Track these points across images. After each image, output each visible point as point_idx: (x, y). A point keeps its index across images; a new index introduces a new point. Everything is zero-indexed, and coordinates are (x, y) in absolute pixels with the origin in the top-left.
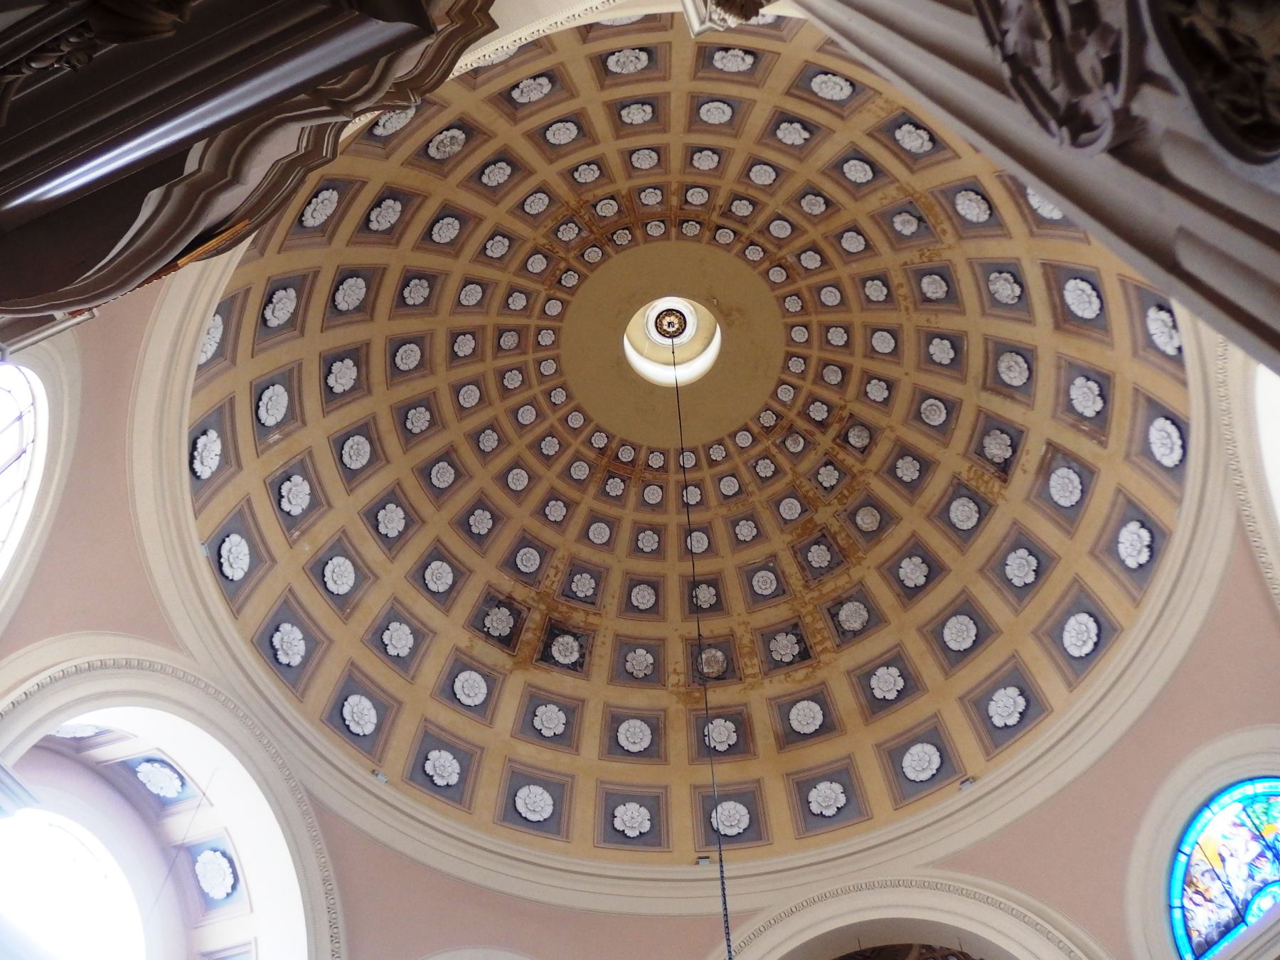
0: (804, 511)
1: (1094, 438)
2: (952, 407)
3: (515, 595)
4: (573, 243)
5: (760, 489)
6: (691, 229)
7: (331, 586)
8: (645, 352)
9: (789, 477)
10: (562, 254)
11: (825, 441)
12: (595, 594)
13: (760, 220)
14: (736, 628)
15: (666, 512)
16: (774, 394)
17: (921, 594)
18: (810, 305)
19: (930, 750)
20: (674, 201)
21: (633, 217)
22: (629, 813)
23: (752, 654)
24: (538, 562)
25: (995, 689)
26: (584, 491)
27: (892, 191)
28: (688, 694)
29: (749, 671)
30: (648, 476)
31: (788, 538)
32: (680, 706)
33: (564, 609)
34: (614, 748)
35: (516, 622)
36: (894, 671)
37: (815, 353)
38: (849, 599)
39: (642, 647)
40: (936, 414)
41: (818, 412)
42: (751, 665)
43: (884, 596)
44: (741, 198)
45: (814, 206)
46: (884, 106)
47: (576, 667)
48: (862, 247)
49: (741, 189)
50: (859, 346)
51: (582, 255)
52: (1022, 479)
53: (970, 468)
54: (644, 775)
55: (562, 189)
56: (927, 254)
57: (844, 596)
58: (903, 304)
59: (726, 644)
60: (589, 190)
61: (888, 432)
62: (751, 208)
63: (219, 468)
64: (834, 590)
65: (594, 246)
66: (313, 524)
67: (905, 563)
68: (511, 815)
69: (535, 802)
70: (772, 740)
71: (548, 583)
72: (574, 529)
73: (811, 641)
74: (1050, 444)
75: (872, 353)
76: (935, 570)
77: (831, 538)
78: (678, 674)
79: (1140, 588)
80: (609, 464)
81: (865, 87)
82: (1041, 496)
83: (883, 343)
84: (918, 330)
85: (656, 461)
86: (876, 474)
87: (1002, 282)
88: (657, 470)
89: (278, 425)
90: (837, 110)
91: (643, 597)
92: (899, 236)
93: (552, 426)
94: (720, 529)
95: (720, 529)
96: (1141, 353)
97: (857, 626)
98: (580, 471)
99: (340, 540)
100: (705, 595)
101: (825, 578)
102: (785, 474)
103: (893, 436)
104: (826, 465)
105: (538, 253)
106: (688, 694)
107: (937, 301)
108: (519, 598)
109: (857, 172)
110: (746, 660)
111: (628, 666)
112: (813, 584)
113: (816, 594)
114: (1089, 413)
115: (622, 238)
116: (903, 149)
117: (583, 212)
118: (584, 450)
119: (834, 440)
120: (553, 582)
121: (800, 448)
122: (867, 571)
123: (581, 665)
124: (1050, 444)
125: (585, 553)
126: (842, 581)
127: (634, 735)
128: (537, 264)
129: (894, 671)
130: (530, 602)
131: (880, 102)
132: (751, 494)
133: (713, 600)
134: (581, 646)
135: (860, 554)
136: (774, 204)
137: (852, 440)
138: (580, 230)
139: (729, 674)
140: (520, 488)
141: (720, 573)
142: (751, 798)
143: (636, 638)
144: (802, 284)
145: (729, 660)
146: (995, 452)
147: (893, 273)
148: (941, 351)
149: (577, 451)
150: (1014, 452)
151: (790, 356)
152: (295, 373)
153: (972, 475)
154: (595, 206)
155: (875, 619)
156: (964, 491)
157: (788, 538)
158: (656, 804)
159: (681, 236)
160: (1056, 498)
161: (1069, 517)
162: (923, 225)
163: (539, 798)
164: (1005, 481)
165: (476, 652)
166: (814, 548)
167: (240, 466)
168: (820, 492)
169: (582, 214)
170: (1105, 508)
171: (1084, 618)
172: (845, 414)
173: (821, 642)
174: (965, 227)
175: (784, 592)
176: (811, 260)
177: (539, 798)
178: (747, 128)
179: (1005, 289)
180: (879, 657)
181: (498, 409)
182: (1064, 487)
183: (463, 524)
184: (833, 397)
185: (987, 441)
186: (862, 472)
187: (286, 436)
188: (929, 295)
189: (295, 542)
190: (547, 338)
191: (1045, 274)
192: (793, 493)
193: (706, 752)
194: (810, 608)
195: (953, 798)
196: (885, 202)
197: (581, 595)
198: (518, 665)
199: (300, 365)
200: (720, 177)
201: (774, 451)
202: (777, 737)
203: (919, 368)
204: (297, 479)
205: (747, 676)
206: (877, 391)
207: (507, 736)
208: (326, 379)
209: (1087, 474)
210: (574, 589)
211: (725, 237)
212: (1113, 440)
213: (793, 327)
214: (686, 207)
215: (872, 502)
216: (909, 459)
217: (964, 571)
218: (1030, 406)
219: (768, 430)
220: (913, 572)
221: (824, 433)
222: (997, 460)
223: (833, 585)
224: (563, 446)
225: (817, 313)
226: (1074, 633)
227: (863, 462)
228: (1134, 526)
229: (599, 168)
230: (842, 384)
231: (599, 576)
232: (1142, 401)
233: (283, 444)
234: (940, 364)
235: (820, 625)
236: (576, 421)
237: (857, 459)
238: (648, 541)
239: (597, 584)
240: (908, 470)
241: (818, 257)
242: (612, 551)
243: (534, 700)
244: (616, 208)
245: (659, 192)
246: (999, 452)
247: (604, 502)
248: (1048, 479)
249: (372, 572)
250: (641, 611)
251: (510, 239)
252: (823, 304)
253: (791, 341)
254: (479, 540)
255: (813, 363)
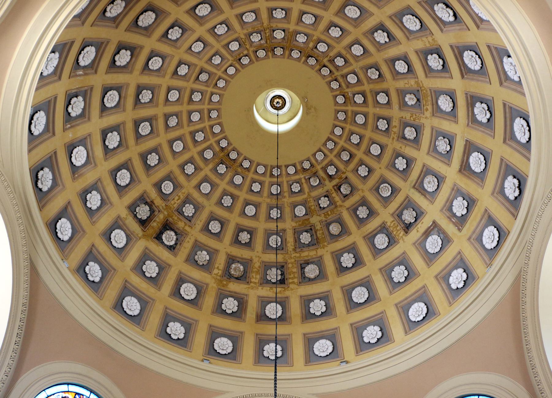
0: (306, 214)
1: (456, 226)
2: (395, 191)
3: (155, 202)
4: (255, 43)
5: (289, 197)
6: (312, 61)
7: (73, 159)
8: (260, 112)
9: (305, 196)
10: (248, 47)
11: (329, 185)
12: (192, 217)
13: (345, 71)
14: (254, 258)
15: (241, 190)
16: (314, 155)
17: (347, 272)
18: (349, 119)
19: (329, 343)
20: (311, 45)
21: (289, 44)
22: (175, 327)
23: (257, 272)
24: (171, 190)
25: (368, 325)
26: (207, 165)
27: (412, 82)
28: (221, 281)
29: (253, 280)
30: (239, 170)
31: (294, 224)
32: (215, 285)
33: (176, 218)
34: (176, 293)
35: (151, 215)
36: (323, 303)
37: (342, 143)
38: (312, 263)
39: (206, 250)
40: (386, 192)
41: (331, 171)
42: (256, 278)
43: (330, 266)
44: (341, 57)
45: (373, 74)
46: (431, 41)
47: (171, 248)
48: (385, 102)
49: (344, 52)
50: (363, 147)
51: (256, 52)
52: (415, 234)
53: (393, 221)
54: (188, 311)
55: (264, 15)
56: (414, 117)
57: (311, 261)
58: (393, 135)
59: (247, 263)
60: (277, 22)
61: (360, 192)
62: (344, 63)
63: (52, 74)
64: (306, 256)
65: (264, 50)
66: (78, 125)
67: (345, 255)
68: (118, 307)
69: (132, 305)
70: (254, 316)
71: (173, 202)
72: (195, 182)
73: (287, 276)
74: (434, 222)
75: (368, 152)
76: (358, 262)
77: (316, 232)
78: (219, 270)
79: (454, 298)
80: (223, 157)
81: (428, 28)
82: (421, 245)
83: (375, 150)
84: (394, 150)
85: (246, 164)
86: (348, 209)
87: (443, 142)
88: (245, 169)
89: (85, 67)
90: (478, 22)
91: (215, 227)
92: (405, 104)
93: (205, 127)
94: (263, 209)
95: (263, 209)
96: (495, 194)
97: (312, 276)
98: (209, 155)
99: (85, 138)
100: (244, 237)
101: (304, 249)
102: (305, 194)
103: (362, 195)
104: (325, 196)
105: (237, 41)
106: (221, 281)
107: (409, 140)
108: (156, 204)
109: (401, 67)
110: (254, 275)
111: (196, 257)
112: (298, 250)
113: (298, 255)
114: (459, 214)
115: (279, 51)
116: (428, 64)
117: (267, 31)
118: (215, 145)
119: (333, 186)
120: (175, 203)
121: (316, 184)
122: (326, 253)
123: (174, 248)
124: (434, 222)
125: (195, 195)
126: (312, 253)
127: (189, 291)
128: (234, 46)
129: (323, 303)
130: (161, 208)
131: (430, 39)
132: (285, 197)
133: (248, 241)
134: (177, 239)
135: (326, 244)
136: (355, 66)
137: (342, 189)
138: (262, 39)
139: (242, 278)
140: (177, 151)
141: (256, 229)
142: (236, 339)
143: (205, 245)
144: (350, 108)
145: (245, 271)
146: (407, 218)
147: (394, 120)
148: (401, 164)
149: (211, 144)
150: (415, 221)
151: (329, 139)
152: (104, 45)
153: (392, 225)
154: (274, 31)
155: (322, 276)
156: (385, 231)
157: (294, 224)
158: (189, 327)
159: (306, 62)
160: (427, 248)
161: (430, 258)
162: (418, 103)
163: (134, 304)
164: (406, 233)
165: (127, 222)
166: (304, 233)
167: (60, 78)
168: (318, 208)
169: (267, 33)
170: (450, 259)
171: (422, 305)
172: (344, 176)
173: (292, 278)
174: (437, 110)
175: (283, 249)
176: (359, 99)
177: (134, 304)
178: (363, 25)
179: (443, 146)
180: (318, 294)
181: (184, 108)
182: (433, 243)
183: (144, 157)
184: (341, 166)
185: (405, 212)
186: (341, 206)
187: (86, 74)
188: (406, 136)
189: (66, 129)
190: (221, 84)
191: (465, 145)
192: (304, 204)
193: (219, 310)
194: (293, 260)
195: (334, 367)
196: (407, 86)
197: (186, 214)
198: (144, 236)
199: (108, 42)
200: (338, 43)
201: (303, 181)
202: (257, 316)
203: (387, 167)
204: (80, 98)
205: (251, 282)
206: (363, 171)
207: (129, 269)
208: (115, 55)
209: (446, 241)
210: (184, 210)
211: (325, 72)
212: (465, 230)
213: (336, 127)
214: (315, 50)
215: (340, 221)
216: (365, 208)
217: (372, 268)
218: (432, 203)
219: (304, 170)
220: (347, 260)
221: (330, 181)
222: (406, 222)
223: (307, 254)
224: (206, 139)
225: (351, 124)
226: (415, 310)
227: (343, 201)
228: (461, 271)
229: (286, 14)
230: (348, 162)
231: (198, 208)
232: (486, 216)
233: (82, 78)
234: (398, 169)
235: (295, 270)
236: (217, 129)
237: (341, 199)
238: (227, 201)
239: (195, 212)
240: (363, 212)
241: (363, 99)
242: (208, 199)
243: (145, 257)
244: (283, 36)
245: (306, 38)
246: (409, 219)
247: (214, 174)
248: (427, 238)
249: (94, 162)
250: (212, 233)
251: (228, 28)
252: (355, 122)
253: (333, 132)
254: (148, 168)
255: (339, 147)
